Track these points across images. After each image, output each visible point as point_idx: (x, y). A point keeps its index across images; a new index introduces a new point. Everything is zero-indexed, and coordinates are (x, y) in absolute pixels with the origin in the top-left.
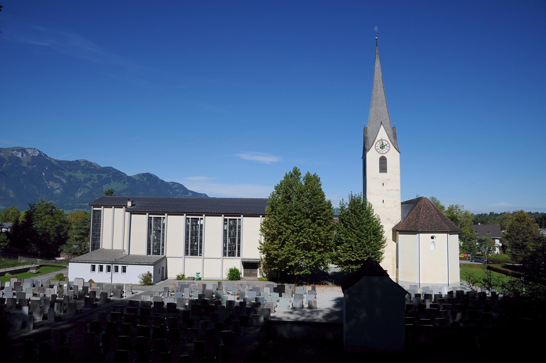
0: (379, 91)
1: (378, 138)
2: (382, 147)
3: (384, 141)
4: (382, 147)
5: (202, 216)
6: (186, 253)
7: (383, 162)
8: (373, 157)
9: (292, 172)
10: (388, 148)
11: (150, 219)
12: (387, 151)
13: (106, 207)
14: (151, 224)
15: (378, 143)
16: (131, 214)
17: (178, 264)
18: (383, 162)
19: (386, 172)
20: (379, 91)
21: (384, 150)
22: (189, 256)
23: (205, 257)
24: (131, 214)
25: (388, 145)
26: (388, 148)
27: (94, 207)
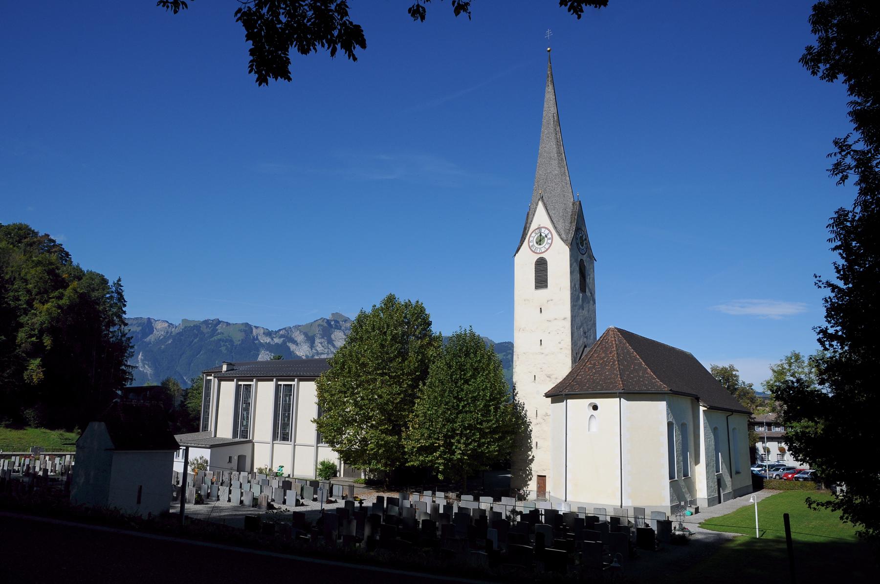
0: (548, 145)
1: (534, 226)
2: (540, 241)
3: (543, 230)
4: (540, 241)
5: (293, 380)
6: (275, 437)
7: (541, 266)
8: (524, 263)
9: (824, 324)
10: (550, 241)
11: (278, 387)
12: (547, 246)
13: (303, 378)
14: (694, 433)
15: (533, 235)
16: (220, 381)
17: (266, 454)
18: (541, 266)
19: (546, 287)
20: (548, 145)
21: (545, 245)
22: (278, 442)
23: (297, 442)
24: (220, 381)
25: (549, 236)
26: (550, 241)
27: (207, 375)
